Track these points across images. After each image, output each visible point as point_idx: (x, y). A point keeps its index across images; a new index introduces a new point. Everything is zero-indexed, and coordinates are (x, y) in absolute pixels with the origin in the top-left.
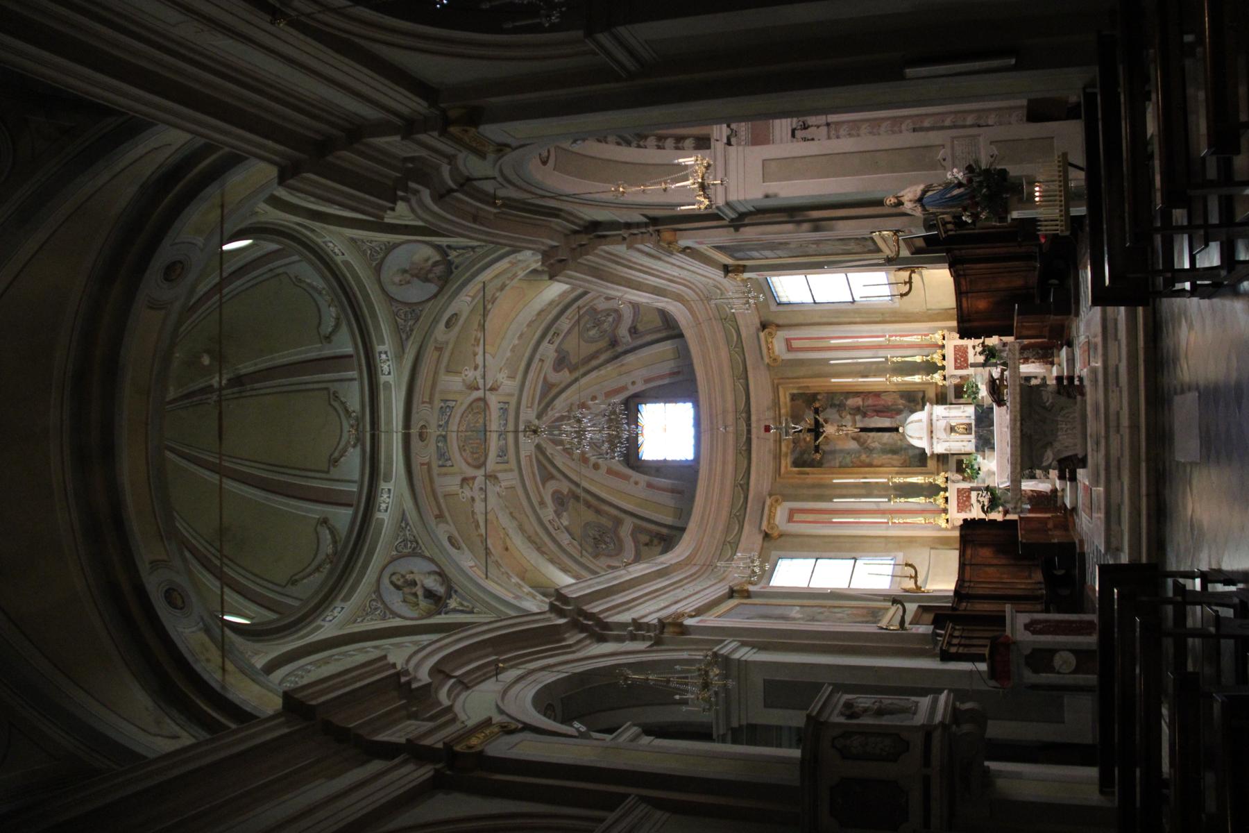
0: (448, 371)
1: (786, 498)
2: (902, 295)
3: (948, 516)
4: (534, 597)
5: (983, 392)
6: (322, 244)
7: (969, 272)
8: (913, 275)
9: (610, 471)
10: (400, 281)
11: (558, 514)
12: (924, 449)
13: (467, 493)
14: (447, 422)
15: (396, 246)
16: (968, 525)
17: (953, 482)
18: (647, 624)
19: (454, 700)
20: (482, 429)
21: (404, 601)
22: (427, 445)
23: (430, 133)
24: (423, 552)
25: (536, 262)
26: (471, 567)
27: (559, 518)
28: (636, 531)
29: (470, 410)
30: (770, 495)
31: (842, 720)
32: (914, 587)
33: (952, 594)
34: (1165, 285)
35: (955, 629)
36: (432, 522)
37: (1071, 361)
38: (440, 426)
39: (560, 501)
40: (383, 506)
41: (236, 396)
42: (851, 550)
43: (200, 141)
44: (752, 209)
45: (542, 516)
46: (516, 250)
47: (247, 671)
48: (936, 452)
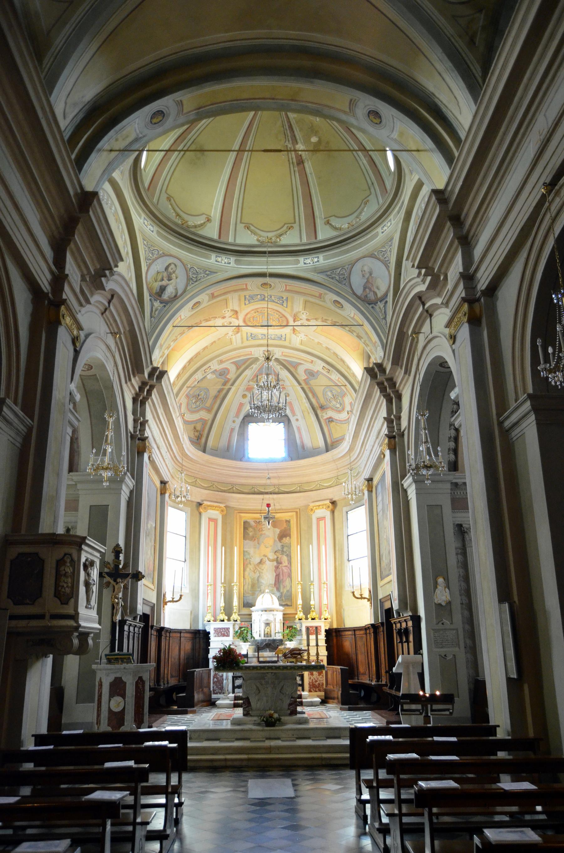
0: (306, 302)
1: (224, 518)
2: (353, 593)
3: (212, 622)
4: (162, 357)
5: (290, 645)
6: (389, 219)
8: (366, 600)
9: (241, 405)
11: (214, 372)
12: (254, 606)
13: (228, 314)
14: (274, 301)
15: (387, 267)
16: (205, 635)
17: (234, 625)
18: (145, 430)
19: (94, 305)
20: (269, 324)
21: (158, 273)
22: (259, 288)
23: (464, 291)
25: (376, 359)
26: (180, 316)
27: (212, 372)
28: (204, 422)
29: (281, 316)
30: (226, 507)
31: (83, 560)
33: (162, 625)
34: (366, 781)
35: (139, 628)
36: (209, 292)
37: (311, 704)
38: (271, 297)
39: (223, 373)
40: (219, 259)
43: (463, 135)
45: (213, 362)
46: (384, 347)
47: (110, 167)
48: (253, 613)
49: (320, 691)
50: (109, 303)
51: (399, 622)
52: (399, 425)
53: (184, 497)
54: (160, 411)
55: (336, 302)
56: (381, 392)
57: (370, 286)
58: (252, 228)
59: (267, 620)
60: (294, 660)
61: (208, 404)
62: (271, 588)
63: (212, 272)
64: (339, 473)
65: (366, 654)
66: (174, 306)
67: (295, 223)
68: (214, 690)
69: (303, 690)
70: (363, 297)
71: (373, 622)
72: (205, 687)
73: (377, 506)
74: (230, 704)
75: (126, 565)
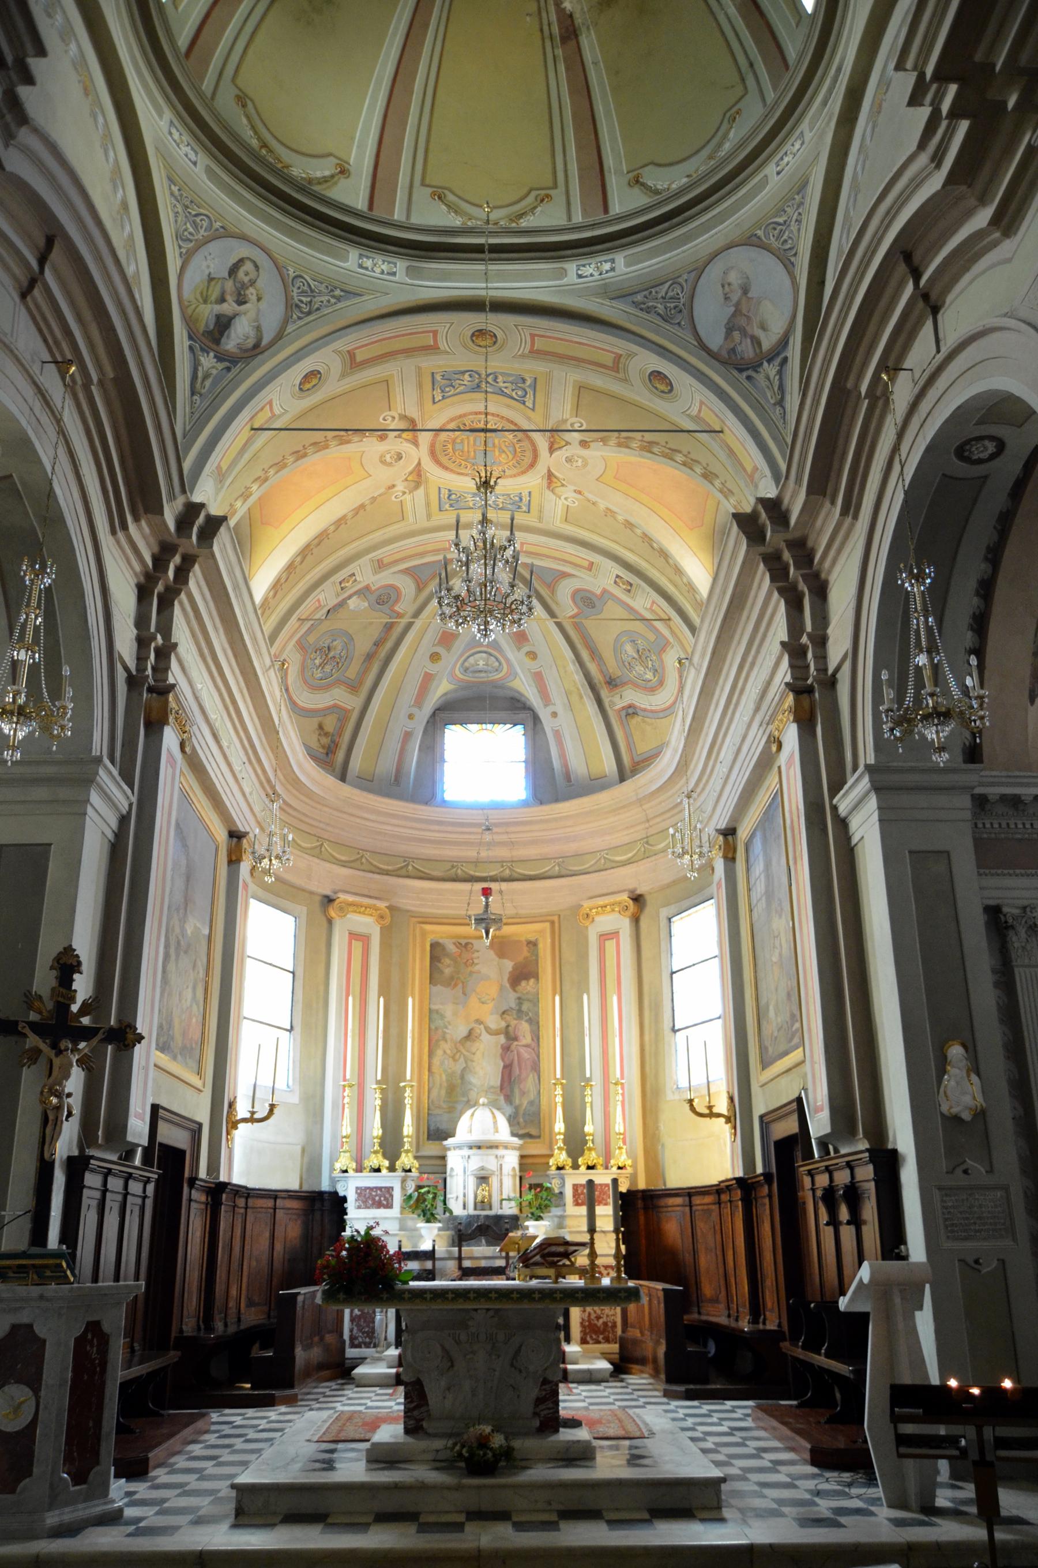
0: (581, 389)
1: (386, 933)
3: (351, 1172)
5: (538, 1230)
7: (727, 1211)
8: (722, 1120)
9: (428, 679)
10: (729, 284)
11: (364, 592)
12: (453, 1135)
16: (338, 1203)
17: (404, 1181)
18: (167, 668)
21: (211, 279)
24: (295, 322)
26: (270, 403)
28: (341, 714)
30: (391, 908)
32: (239, 1117)
33: (223, 1178)
37: (590, 1378)
38: (495, 380)
39: (385, 598)
40: (368, 263)
41: (546, 28)
42: (307, 1026)
44: (855, 840)
49: (607, 1340)
50: (42, 261)
51: (827, 1169)
52: (822, 657)
53: (277, 857)
54: (219, 641)
55: (657, 376)
56: (773, 579)
57: (743, 322)
58: (451, 197)
59: (482, 1168)
60: (551, 1272)
61: (352, 672)
62: (494, 1097)
63: (349, 294)
64: (652, 831)
65: (719, 1253)
66: (254, 370)
67: (555, 186)
68: (352, 1338)
69: (568, 1340)
70: (724, 353)
71: (740, 1173)
72: (329, 1332)
73: (749, 890)
74: (387, 1376)
75: (94, 1006)
